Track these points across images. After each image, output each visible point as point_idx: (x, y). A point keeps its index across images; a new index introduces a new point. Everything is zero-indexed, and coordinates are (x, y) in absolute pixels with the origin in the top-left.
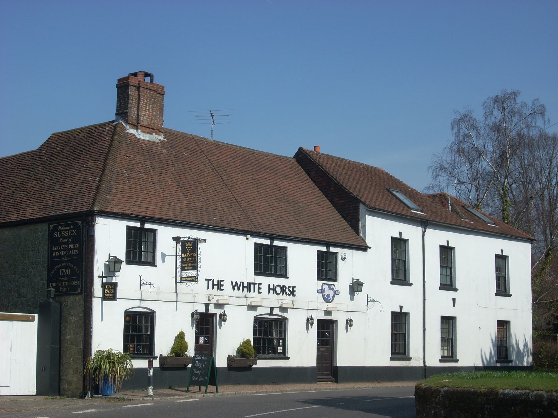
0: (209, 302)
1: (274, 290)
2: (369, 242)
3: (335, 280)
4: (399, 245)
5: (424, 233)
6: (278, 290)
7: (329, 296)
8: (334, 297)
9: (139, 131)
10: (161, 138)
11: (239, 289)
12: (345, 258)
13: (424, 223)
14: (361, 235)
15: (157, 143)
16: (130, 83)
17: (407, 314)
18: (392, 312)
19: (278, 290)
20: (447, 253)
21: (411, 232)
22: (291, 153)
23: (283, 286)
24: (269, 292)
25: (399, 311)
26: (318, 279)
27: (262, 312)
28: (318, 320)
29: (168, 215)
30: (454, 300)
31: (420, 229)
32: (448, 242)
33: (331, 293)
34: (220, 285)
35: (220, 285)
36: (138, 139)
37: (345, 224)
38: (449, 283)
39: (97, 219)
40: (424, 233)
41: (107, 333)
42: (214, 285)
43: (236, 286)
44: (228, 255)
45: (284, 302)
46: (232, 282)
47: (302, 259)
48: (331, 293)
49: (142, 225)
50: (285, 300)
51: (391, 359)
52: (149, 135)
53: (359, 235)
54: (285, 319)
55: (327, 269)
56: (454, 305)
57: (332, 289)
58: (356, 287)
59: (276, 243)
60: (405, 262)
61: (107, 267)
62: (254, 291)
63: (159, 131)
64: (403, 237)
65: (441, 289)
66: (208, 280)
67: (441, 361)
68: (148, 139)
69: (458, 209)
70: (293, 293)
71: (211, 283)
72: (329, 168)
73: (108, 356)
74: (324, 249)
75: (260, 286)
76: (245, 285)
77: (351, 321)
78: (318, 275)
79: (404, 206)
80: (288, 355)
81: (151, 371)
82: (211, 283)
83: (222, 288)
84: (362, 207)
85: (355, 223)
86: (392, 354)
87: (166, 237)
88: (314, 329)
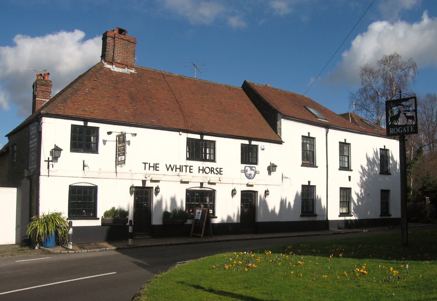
0: (145, 179)
1: (204, 170)
2: (283, 139)
3: (256, 164)
4: (308, 142)
5: (327, 133)
6: (207, 170)
7: (250, 175)
8: (254, 175)
9: (114, 66)
10: (133, 71)
11: (172, 170)
12: (263, 149)
13: (327, 127)
14: (279, 134)
15: (128, 74)
16: (107, 35)
17: (314, 187)
18: (302, 185)
19: (207, 170)
20: (344, 147)
21: (317, 132)
22: (240, 85)
23: (212, 168)
24: (158, 170)
25: (307, 184)
26: (243, 162)
27: (194, 185)
28: (242, 191)
29: (109, 118)
30: (350, 177)
31: (323, 130)
32: (385, 146)
33: (253, 173)
34: (155, 167)
35: (155, 167)
36: (112, 71)
37: (268, 127)
38: (346, 166)
39: (43, 118)
40: (327, 133)
41: (53, 200)
42: (150, 167)
43: (169, 168)
44: (170, 145)
45: (211, 179)
46: (166, 165)
47: (228, 149)
48: (253, 173)
49: (86, 123)
50: (213, 177)
51: (301, 216)
52: (122, 69)
53: (277, 134)
54: (214, 191)
55: (249, 156)
56: (350, 180)
57: (254, 170)
58: (272, 168)
59: (90, 124)
60: (313, 152)
61: (52, 153)
62: (186, 171)
63: (131, 67)
64: (310, 136)
65: (339, 170)
66: (145, 163)
67: (339, 216)
68: (120, 71)
69: (356, 121)
70: (220, 172)
71: (147, 166)
72: (259, 91)
73: (54, 218)
74: (247, 142)
75: (191, 168)
76: (178, 167)
77: (268, 191)
78: (303, 159)
79: (313, 116)
80: (216, 215)
81: (71, 231)
82: (147, 166)
83: (157, 169)
84: (279, 115)
85: (274, 126)
86: (302, 212)
87: (107, 133)
88: (238, 196)
